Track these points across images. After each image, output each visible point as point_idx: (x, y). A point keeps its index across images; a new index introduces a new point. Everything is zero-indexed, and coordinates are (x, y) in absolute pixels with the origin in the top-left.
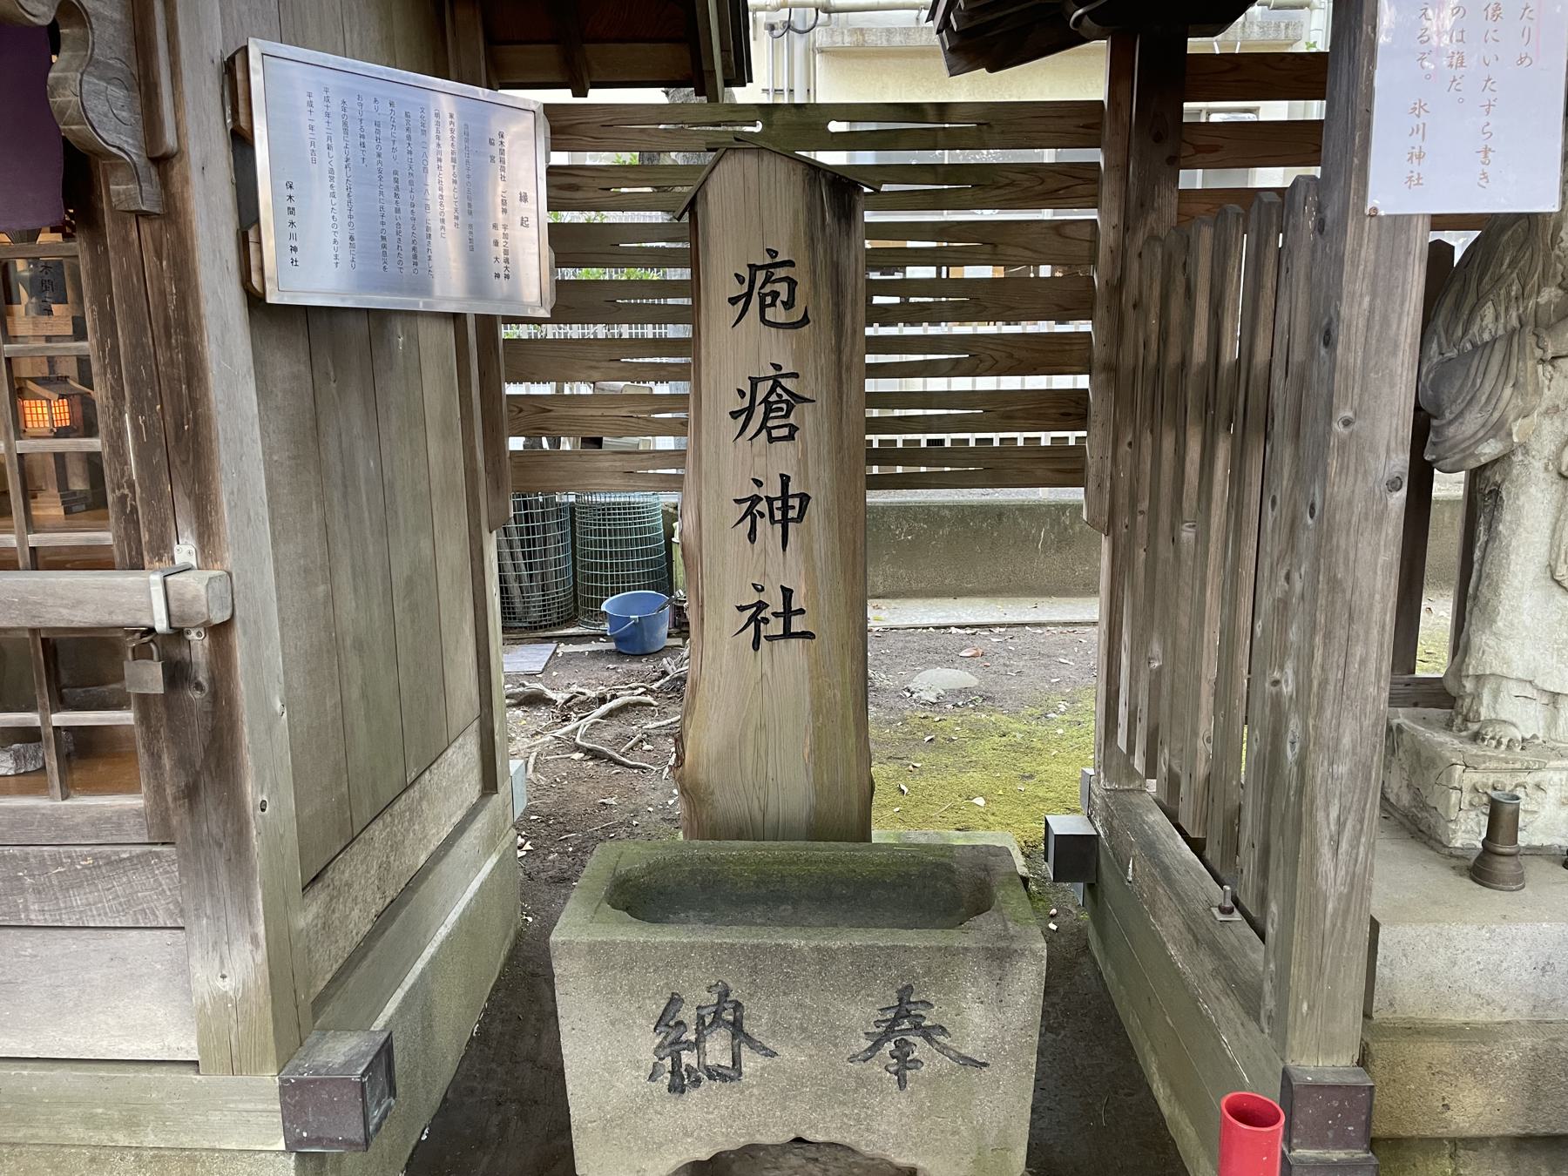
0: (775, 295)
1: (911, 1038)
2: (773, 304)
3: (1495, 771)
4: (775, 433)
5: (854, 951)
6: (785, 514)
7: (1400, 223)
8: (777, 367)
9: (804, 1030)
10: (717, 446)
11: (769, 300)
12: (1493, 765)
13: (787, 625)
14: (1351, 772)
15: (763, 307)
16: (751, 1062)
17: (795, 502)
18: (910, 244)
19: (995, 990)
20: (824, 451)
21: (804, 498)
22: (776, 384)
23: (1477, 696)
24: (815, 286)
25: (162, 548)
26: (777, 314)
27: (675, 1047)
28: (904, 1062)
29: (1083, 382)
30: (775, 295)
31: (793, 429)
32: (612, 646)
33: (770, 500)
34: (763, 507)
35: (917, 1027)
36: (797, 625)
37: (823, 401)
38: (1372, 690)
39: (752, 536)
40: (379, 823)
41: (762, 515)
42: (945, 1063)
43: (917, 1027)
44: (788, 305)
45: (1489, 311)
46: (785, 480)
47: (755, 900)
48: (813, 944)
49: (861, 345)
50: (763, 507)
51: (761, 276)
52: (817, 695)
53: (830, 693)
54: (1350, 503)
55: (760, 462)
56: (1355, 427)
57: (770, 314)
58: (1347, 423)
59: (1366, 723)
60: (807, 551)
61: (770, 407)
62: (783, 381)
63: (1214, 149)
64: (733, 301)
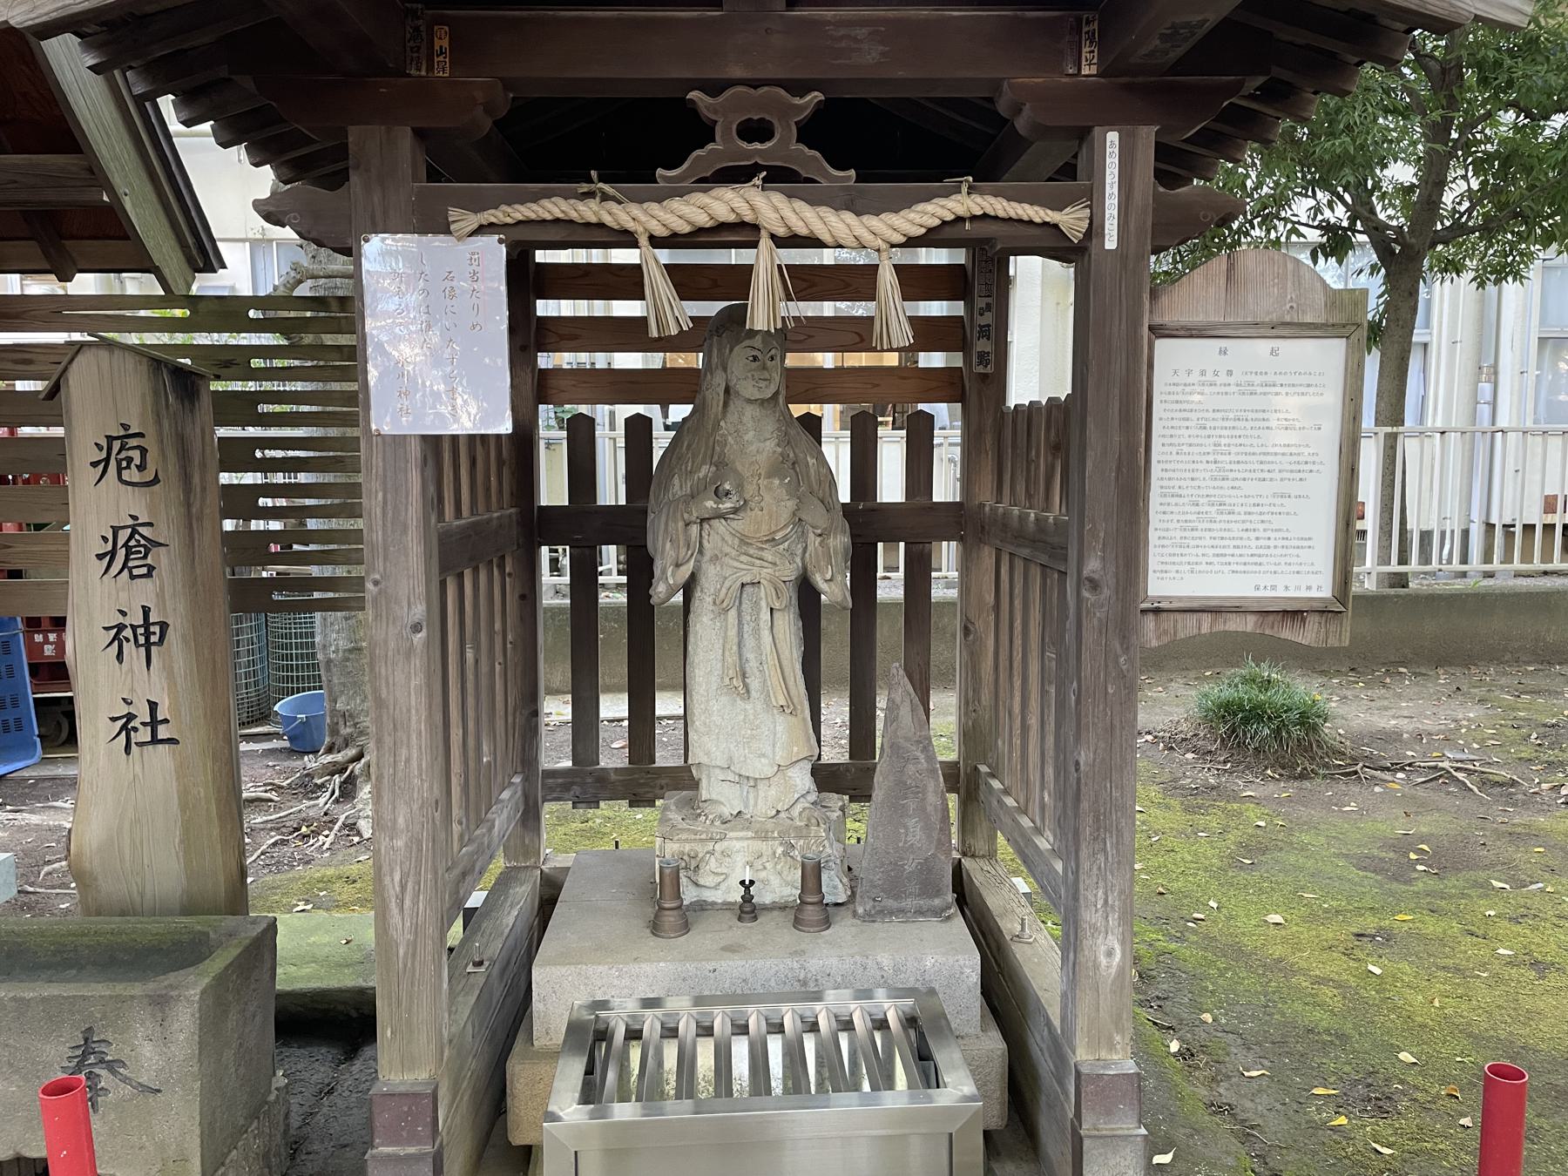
1: (96, 1070)
2: (128, 467)
4: (135, 572)
5: (44, 1000)
6: (148, 639)
7: (399, 441)
8: (134, 518)
9: (11, 1065)
10: (86, 583)
11: (124, 464)
12: (684, 836)
13: (154, 733)
14: (406, 845)
15: (120, 470)
17: (156, 629)
19: (158, 1029)
20: (179, 587)
21: (164, 626)
22: (134, 532)
26: (132, 475)
31: (151, 568)
32: (287, 744)
33: (134, 628)
34: (128, 633)
35: (102, 1061)
37: (175, 544)
41: (128, 640)
43: (102, 1061)
44: (141, 468)
45: (676, 481)
46: (146, 611)
47: (48, 966)
48: (11, 995)
49: (214, 502)
50: (128, 633)
51: (116, 445)
52: (184, 794)
54: (386, 642)
55: (123, 595)
56: (382, 586)
57: (126, 475)
58: (376, 583)
59: (415, 807)
62: (140, 529)
63: (575, 337)
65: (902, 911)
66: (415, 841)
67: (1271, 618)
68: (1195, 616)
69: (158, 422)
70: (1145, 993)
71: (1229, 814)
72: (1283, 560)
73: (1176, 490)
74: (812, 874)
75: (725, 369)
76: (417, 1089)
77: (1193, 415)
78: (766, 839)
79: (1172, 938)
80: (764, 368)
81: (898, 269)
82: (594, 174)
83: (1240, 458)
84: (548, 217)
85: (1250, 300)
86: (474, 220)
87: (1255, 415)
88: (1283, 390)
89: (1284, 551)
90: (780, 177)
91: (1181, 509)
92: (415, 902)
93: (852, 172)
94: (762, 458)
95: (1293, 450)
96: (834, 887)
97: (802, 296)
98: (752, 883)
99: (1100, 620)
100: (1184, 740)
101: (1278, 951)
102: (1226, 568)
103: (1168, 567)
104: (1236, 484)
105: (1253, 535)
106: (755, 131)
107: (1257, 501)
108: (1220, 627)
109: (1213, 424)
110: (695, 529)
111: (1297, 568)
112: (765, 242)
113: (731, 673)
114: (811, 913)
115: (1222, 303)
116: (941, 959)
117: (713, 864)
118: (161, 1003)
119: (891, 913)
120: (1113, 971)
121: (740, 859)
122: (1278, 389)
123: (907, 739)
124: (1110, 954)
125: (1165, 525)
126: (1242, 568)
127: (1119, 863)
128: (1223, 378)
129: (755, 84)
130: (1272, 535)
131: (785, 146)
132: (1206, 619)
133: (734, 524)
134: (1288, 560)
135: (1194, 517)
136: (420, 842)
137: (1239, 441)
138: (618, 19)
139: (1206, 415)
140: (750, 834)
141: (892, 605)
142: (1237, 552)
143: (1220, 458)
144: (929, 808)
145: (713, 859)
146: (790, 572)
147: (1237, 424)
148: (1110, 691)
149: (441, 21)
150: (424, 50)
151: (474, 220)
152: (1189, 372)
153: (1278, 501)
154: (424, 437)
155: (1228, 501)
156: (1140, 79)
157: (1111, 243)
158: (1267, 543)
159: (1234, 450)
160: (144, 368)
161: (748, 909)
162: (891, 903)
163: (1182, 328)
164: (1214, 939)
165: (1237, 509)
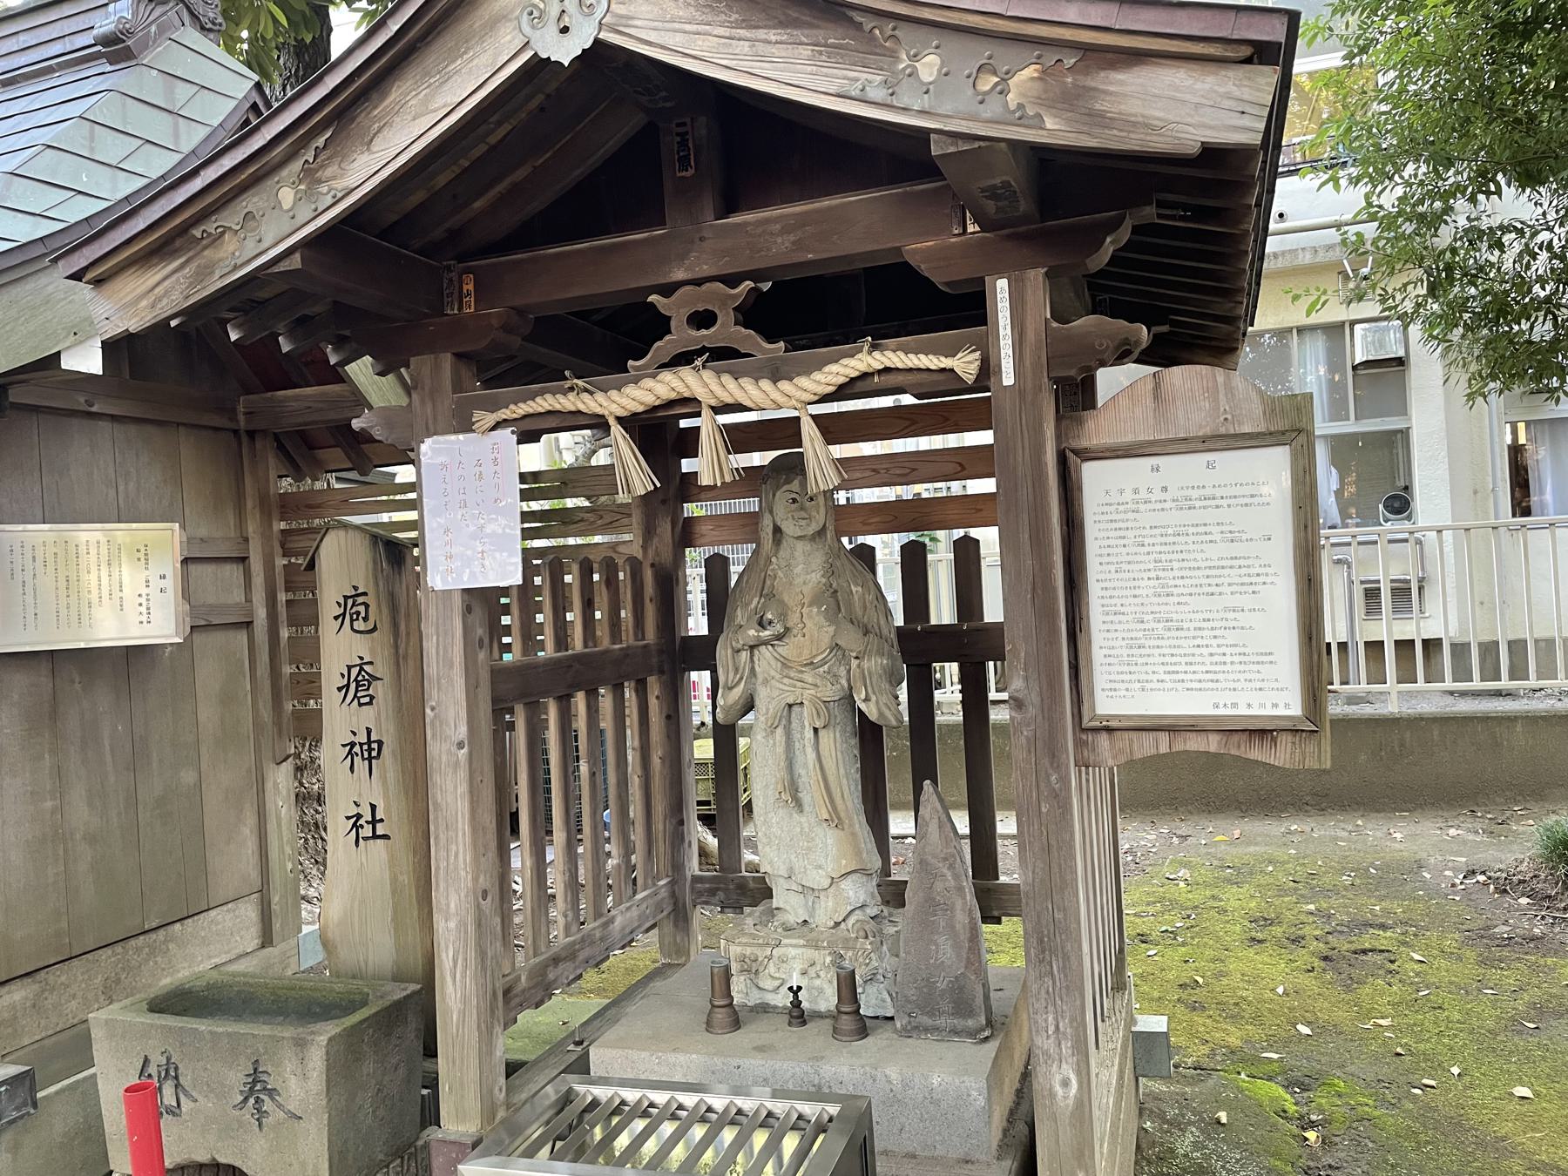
0: (358, 613)
3: (746, 944)
5: (229, 1035)
7: (447, 593)
15: (352, 621)
17: (375, 746)
21: (380, 743)
22: (362, 669)
24: (379, 606)
28: (260, 1114)
30: (358, 613)
33: (361, 745)
34: (357, 749)
37: (387, 679)
38: (463, 873)
40: (109, 951)
43: (265, 1089)
44: (365, 619)
46: (369, 731)
47: (266, 1013)
51: (350, 602)
52: (394, 880)
53: (401, 878)
58: (433, 709)
64: (336, 618)
65: (936, 1029)
66: (462, 924)
67: (1236, 738)
68: (1151, 735)
69: (377, 584)
70: (1319, 1159)
71: (1535, 969)
72: (1242, 677)
73: (1119, 608)
74: (848, 986)
75: (771, 512)
76: (463, 1140)
77: (1130, 534)
78: (817, 948)
79: (1383, 1102)
80: (802, 508)
81: (816, 418)
82: (567, 373)
83: (1184, 573)
84: (541, 410)
85: (1180, 414)
86: (491, 418)
87: (1195, 530)
88: (1224, 502)
89: (1242, 667)
90: (721, 355)
91: (1126, 627)
92: (464, 976)
93: (782, 344)
94: (806, 590)
95: (1242, 562)
96: (872, 1001)
97: (738, 450)
98: (800, 988)
99: (1028, 739)
100: (1521, 882)
101: (1505, 1128)
102: (1179, 686)
103: (1117, 686)
104: (1182, 599)
105: (1205, 651)
106: (703, 319)
107: (1206, 616)
108: (1179, 746)
109: (1151, 541)
110: (744, 655)
111: (1259, 685)
112: (706, 412)
113: (780, 788)
114: (847, 1022)
115: (1151, 421)
116: (948, 1079)
117: (772, 969)
118: (301, 1044)
119: (926, 1030)
120: (1071, 1102)
121: (798, 966)
122: (1219, 502)
123: (935, 856)
124: (1066, 1083)
125: (1111, 643)
126: (1198, 685)
127: (1067, 987)
128: (1157, 495)
129: (698, 282)
130: (1228, 651)
131: (728, 330)
132: (1164, 738)
133: (780, 650)
134: (1248, 676)
135: (1140, 634)
136: (466, 925)
137: (1181, 556)
138: (590, 248)
139: (1144, 532)
140: (802, 942)
141: (950, 727)
142: (1189, 668)
143: (1161, 574)
144: (958, 926)
145: (771, 964)
146: (830, 692)
147: (1176, 539)
148: (1044, 810)
149: (468, 271)
150: (456, 295)
151: (491, 418)
152: (1122, 492)
153: (1231, 615)
154: (464, 590)
155: (1175, 616)
156: (1023, 229)
157: (1008, 379)
158: (1223, 659)
159: (1176, 565)
160: (367, 542)
161: (798, 1015)
162: (926, 1020)
163: (1108, 450)
164: (1435, 1109)
165: (1185, 625)
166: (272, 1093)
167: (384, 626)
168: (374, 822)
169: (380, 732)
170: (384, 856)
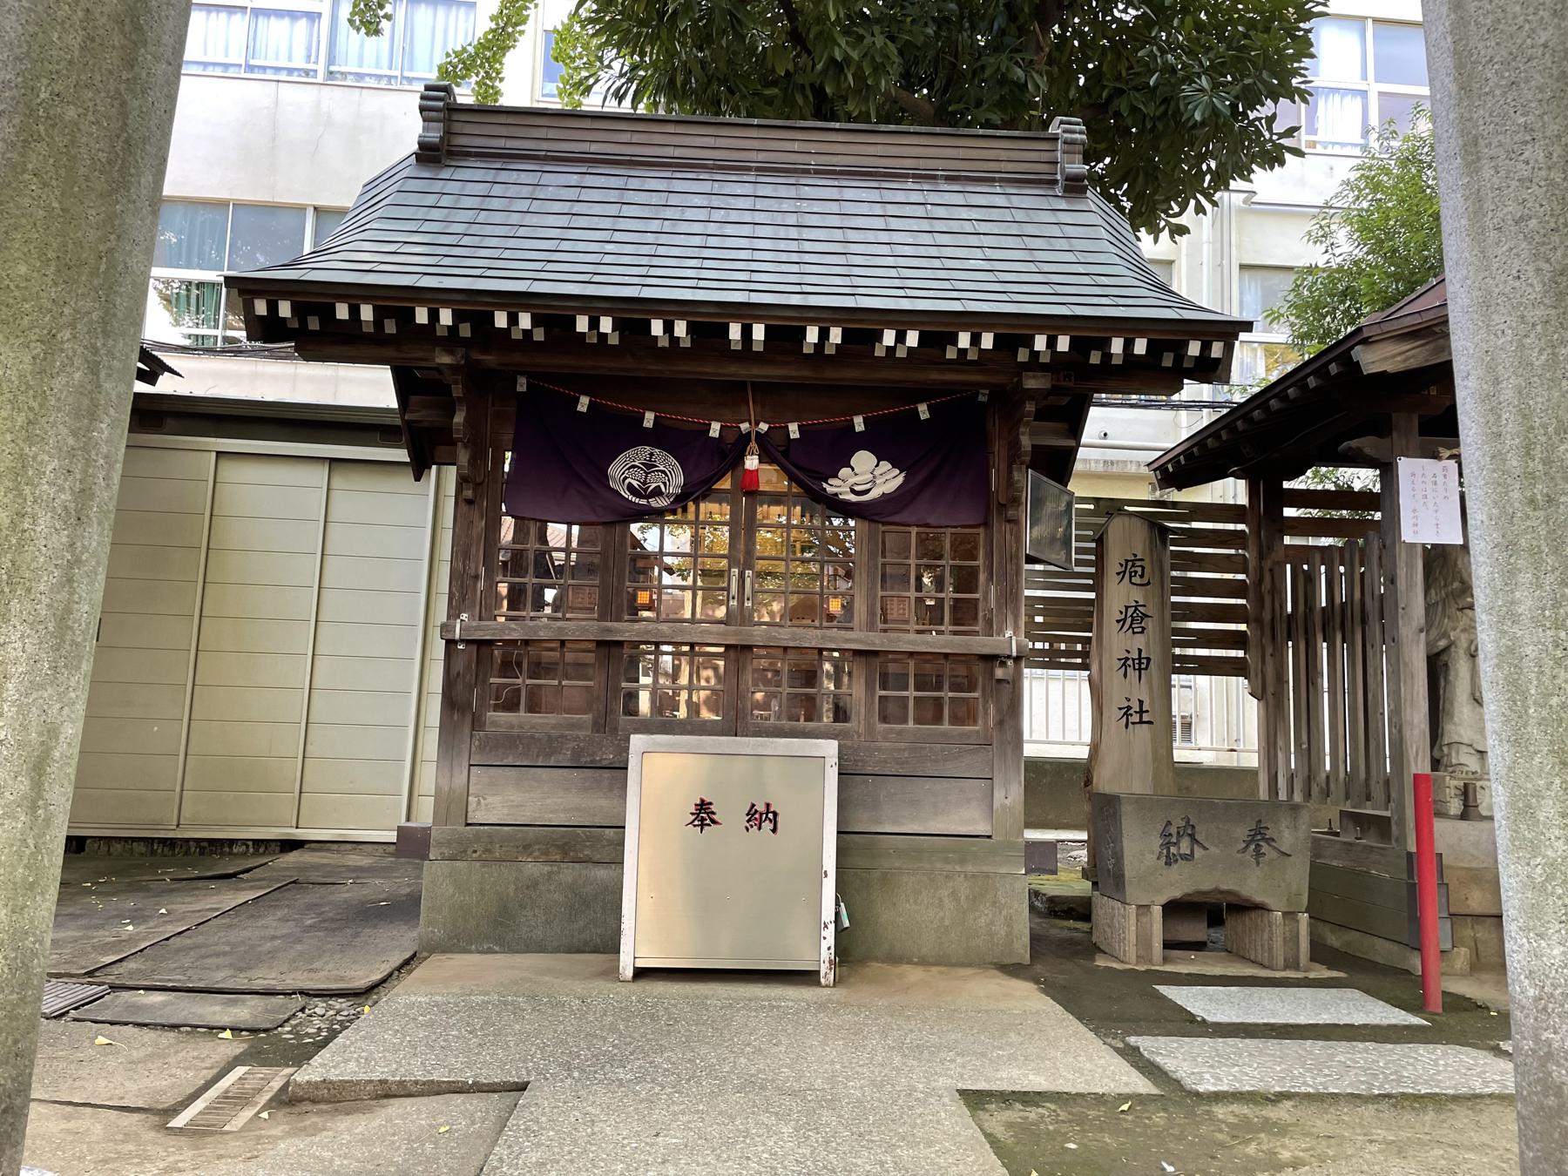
7: (1413, 545)
16: (1198, 852)
18: (1197, 550)
21: (1148, 659)
23: (1449, 755)
25: (1001, 632)
26: (1136, 580)
27: (1167, 845)
28: (1258, 854)
29: (1243, 627)
36: (1146, 717)
39: (1125, 675)
42: (1274, 854)
44: (1142, 576)
60: (1150, 683)
61: (1133, 619)
86: (1448, 453)
166: (1269, 841)
167: (1156, 580)
168: (1141, 712)
169: (1148, 651)
170: (1148, 736)
